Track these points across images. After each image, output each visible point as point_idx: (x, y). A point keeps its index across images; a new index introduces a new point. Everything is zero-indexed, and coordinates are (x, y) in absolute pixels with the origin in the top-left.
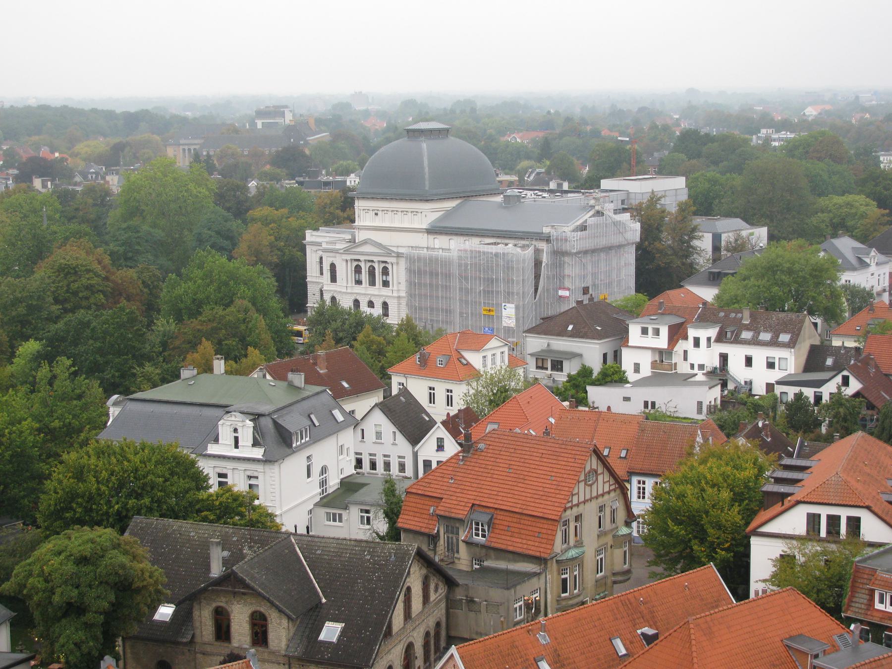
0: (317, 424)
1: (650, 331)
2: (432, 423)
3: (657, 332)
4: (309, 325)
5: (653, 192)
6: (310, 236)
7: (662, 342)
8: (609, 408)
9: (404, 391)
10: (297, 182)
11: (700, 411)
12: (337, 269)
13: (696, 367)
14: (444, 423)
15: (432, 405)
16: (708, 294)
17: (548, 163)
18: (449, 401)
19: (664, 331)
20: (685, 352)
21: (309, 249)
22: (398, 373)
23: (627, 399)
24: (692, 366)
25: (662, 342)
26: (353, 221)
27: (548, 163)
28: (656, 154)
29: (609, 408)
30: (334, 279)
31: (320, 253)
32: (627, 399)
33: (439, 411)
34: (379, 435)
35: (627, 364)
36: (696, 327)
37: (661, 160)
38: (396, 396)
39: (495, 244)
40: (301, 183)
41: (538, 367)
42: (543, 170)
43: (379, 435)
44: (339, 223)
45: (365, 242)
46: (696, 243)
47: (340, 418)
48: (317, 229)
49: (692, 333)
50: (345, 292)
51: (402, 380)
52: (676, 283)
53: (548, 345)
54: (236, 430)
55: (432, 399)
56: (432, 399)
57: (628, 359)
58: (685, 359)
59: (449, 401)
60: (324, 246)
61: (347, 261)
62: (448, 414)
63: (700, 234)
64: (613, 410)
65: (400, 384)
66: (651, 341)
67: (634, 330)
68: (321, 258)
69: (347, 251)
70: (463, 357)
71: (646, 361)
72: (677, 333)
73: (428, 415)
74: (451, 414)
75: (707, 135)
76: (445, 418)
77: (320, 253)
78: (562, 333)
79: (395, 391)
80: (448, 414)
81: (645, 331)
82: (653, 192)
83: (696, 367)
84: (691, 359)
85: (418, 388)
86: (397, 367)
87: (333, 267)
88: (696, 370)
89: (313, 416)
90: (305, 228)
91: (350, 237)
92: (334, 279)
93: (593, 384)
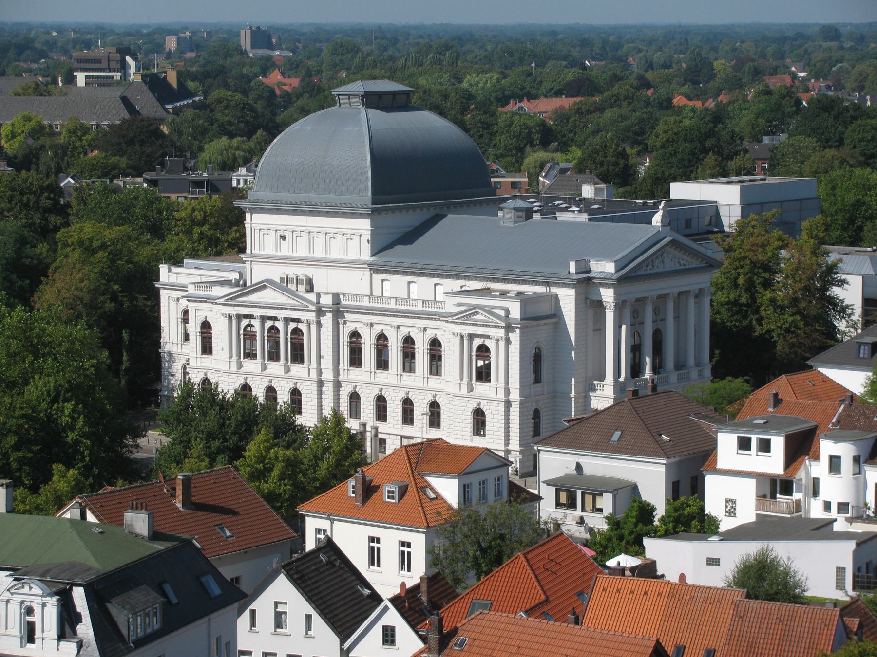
0: (175, 601)
1: (754, 444)
2: (376, 599)
3: (765, 446)
4: (833, 279)
5: (541, 498)
6: (166, 274)
7: (774, 463)
8: (682, 577)
9: (329, 546)
10: (146, 181)
11: (840, 585)
12: (214, 331)
13: (834, 507)
14: (394, 600)
15: (375, 568)
16: (854, 380)
17: (578, 153)
18: (405, 561)
19: (778, 443)
20: (816, 482)
21: (164, 294)
22: (318, 513)
23: (713, 562)
24: (827, 506)
25: (774, 463)
26: (243, 250)
27: (578, 153)
28: (766, 140)
29: (682, 577)
30: (207, 348)
31: (184, 303)
32: (713, 562)
33: (387, 580)
34: (279, 620)
35: (713, 506)
36: (836, 439)
37: (773, 149)
38: (312, 552)
39: (485, 292)
40: (153, 183)
41: (558, 504)
42: (570, 165)
43: (279, 620)
44: (219, 254)
45: (261, 287)
46: (836, 291)
47: (216, 590)
48: (178, 263)
49: (827, 447)
50: (225, 372)
51: (324, 524)
52: (798, 364)
53: (579, 467)
54: (30, 611)
55: (374, 558)
56: (374, 558)
57: (717, 493)
58: (816, 493)
59: (405, 561)
60: (191, 290)
61: (230, 317)
62: (403, 585)
63: (844, 277)
64: (690, 581)
65: (319, 531)
66: (754, 461)
67: (726, 441)
68: (186, 312)
69: (231, 300)
70: (429, 486)
71: (746, 493)
72: (800, 447)
73: (367, 585)
74: (408, 586)
75: (857, 108)
76: (397, 591)
77: (184, 303)
78: (602, 446)
79: (310, 545)
80: (403, 585)
81: (744, 444)
82: (541, 498)
83: (834, 507)
84: (825, 493)
85: (351, 539)
86: (318, 500)
87: (206, 326)
88: (834, 514)
89: (167, 587)
90: (159, 261)
91: (237, 276)
92: (207, 348)
93: (654, 534)
